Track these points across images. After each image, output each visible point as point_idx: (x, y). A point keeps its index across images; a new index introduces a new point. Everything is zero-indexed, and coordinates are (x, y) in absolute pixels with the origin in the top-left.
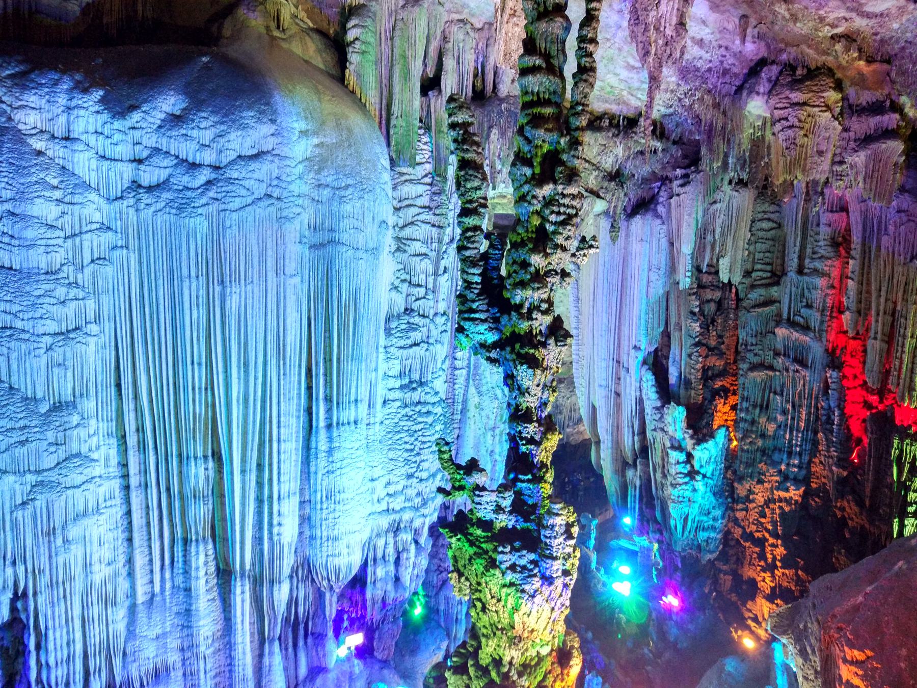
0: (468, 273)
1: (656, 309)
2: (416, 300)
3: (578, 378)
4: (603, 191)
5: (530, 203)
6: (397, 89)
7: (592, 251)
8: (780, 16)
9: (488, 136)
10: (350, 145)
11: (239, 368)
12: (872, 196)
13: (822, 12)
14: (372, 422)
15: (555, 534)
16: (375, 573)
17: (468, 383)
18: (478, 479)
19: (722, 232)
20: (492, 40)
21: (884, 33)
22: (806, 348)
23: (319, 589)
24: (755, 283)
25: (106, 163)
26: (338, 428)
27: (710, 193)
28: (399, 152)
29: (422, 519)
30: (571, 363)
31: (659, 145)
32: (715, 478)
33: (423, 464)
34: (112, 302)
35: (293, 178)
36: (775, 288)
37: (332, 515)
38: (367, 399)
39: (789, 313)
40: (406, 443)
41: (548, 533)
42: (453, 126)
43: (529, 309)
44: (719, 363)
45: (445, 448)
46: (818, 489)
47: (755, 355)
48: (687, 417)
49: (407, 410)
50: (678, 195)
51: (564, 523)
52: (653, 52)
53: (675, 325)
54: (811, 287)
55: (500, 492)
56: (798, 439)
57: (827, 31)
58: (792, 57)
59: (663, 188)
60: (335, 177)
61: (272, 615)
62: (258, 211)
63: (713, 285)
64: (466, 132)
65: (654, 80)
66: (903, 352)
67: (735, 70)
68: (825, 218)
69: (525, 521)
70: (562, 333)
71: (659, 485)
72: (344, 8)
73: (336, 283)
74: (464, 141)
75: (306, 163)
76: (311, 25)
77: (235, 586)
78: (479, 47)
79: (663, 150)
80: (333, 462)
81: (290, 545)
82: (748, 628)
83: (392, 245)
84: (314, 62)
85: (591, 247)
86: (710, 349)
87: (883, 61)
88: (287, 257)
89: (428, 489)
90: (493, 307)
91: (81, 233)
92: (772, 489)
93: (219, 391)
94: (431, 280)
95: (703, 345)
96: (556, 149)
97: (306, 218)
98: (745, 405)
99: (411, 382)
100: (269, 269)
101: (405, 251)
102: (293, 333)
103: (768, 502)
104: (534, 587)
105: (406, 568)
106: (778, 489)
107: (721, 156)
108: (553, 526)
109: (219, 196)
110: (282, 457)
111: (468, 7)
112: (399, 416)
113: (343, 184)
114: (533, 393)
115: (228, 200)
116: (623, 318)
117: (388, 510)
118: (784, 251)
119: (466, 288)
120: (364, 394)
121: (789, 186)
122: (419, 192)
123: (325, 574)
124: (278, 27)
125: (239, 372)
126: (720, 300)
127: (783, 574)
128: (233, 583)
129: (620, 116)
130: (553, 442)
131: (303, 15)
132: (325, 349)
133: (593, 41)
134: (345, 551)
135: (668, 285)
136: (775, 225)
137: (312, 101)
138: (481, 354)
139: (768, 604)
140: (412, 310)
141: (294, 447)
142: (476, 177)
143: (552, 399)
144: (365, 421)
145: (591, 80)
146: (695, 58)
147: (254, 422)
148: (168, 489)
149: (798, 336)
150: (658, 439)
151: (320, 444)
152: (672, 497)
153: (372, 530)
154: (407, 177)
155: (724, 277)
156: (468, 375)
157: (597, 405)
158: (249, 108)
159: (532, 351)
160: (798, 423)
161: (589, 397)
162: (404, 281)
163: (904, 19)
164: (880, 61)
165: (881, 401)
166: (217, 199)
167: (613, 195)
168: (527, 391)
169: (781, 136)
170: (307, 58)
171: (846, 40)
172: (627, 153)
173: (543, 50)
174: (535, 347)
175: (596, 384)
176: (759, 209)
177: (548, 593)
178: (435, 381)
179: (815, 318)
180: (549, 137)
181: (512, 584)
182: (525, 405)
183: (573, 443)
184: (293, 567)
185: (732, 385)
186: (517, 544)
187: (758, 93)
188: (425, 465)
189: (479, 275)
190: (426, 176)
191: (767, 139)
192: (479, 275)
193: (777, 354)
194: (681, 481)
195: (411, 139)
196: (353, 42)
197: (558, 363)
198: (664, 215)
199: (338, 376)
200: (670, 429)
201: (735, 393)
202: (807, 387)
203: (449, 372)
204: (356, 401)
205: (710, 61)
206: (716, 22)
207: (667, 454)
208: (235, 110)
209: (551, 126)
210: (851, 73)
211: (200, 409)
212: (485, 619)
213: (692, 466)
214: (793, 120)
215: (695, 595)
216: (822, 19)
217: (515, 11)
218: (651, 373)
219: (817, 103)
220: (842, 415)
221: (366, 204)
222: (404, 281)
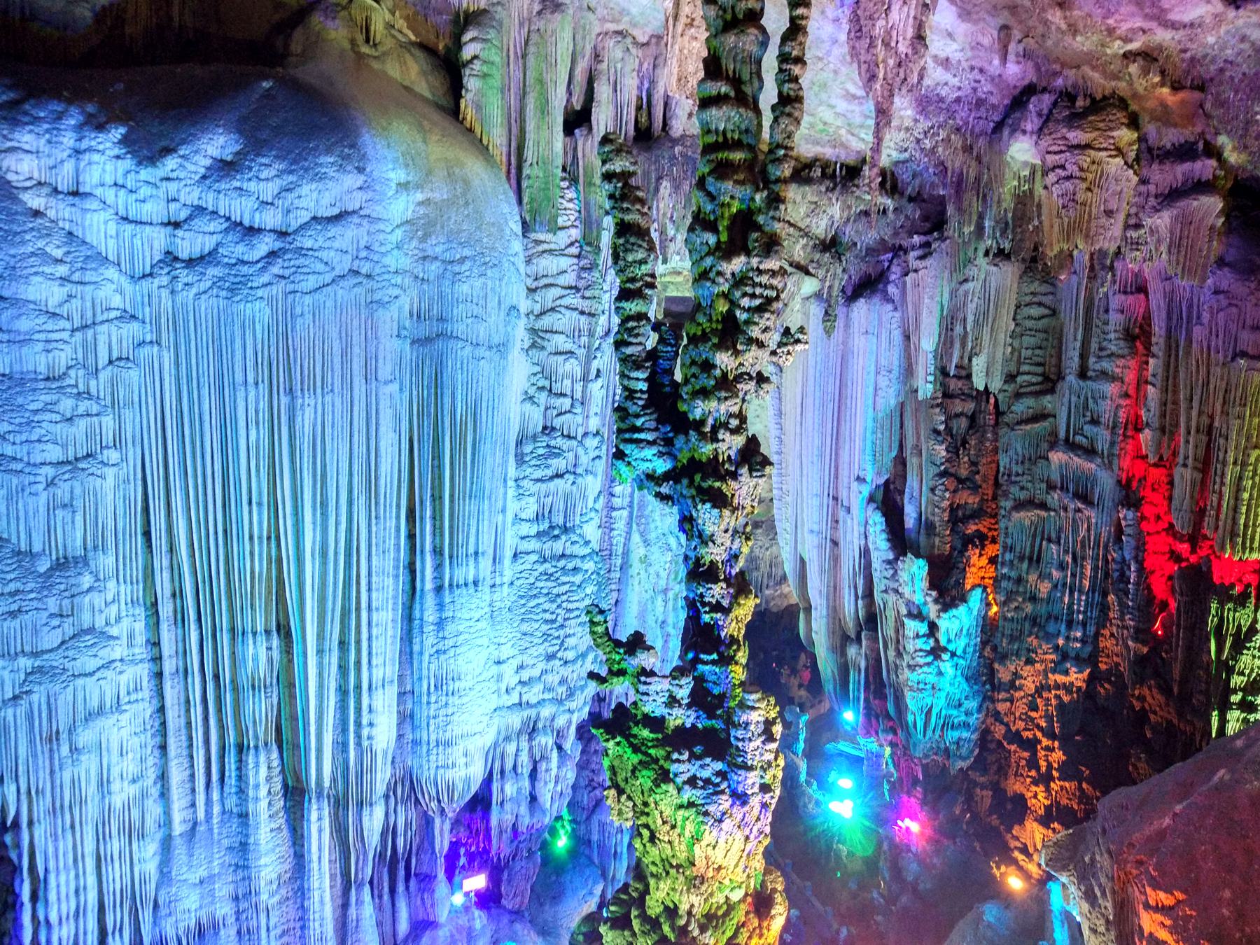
0: (629, 378)
2: (558, 415)
3: (781, 521)
5: (714, 282)
6: (531, 125)
7: (799, 347)
8: (1053, 27)
9: (657, 190)
10: (467, 204)
11: (314, 509)
12: (1179, 271)
13: (1111, 21)
15: (750, 735)
16: (502, 790)
17: (631, 527)
18: (644, 659)
19: (976, 322)
21: (1195, 49)
22: (1093, 480)
24: (1023, 390)
25: (129, 228)
26: (451, 591)
27: (959, 267)
28: (535, 212)
29: (567, 716)
31: (889, 203)
32: (968, 656)
33: (567, 640)
34: (138, 419)
35: (389, 247)
36: (1049, 397)
37: (443, 712)
38: (491, 551)
39: (1068, 431)
40: (545, 611)
42: (608, 177)
43: (713, 427)
44: (972, 500)
45: (599, 618)
46: (1109, 671)
48: (929, 573)
49: (547, 565)
50: (916, 271)
51: (762, 719)
52: (881, 76)
55: (674, 678)
56: (1081, 602)
57: (1117, 47)
58: (1070, 83)
59: (895, 261)
62: (340, 292)
63: (963, 394)
64: (626, 185)
65: (883, 114)
66: (1223, 484)
67: (994, 100)
68: (1116, 301)
70: (759, 459)
71: (892, 666)
72: (458, 14)
73: (447, 393)
74: (624, 197)
75: (407, 227)
76: (413, 38)
79: (895, 209)
80: (444, 638)
81: (385, 753)
83: (526, 339)
84: (417, 89)
85: (798, 341)
86: (960, 481)
87: (1193, 88)
88: (381, 357)
89: (575, 675)
90: (663, 424)
91: (94, 323)
92: (1045, 672)
93: (288, 542)
94: (579, 387)
95: (951, 475)
96: (749, 208)
97: (405, 302)
98: (1008, 556)
99: (552, 528)
100: (356, 372)
101: (543, 348)
103: (1039, 691)
104: (721, 808)
105: (546, 783)
106: (1054, 671)
107: (975, 218)
108: (747, 724)
109: (287, 273)
112: (536, 574)
113: (458, 256)
114: (719, 541)
115: (298, 278)
117: (520, 704)
119: (627, 398)
120: (487, 544)
121: (1067, 258)
122: (562, 266)
123: (434, 793)
124: (367, 41)
125: (314, 515)
127: (1062, 787)
128: (306, 805)
130: (746, 609)
131: (401, 24)
132: (432, 483)
133: (800, 60)
135: (903, 393)
136: (1047, 312)
137: (413, 142)
140: (553, 429)
142: (640, 246)
143: (745, 550)
144: (489, 582)
145: (796, 114)
146: (938, 84)
147: (335, 584)
148: (216, 677)
149: (1079, 462)
151: (426, 614)
153: (499, 732)
154: (545, 246)
155: (979, 382)
157: (807, 560)
158: (328, 151)
159: (717, 484)
160: (1081, 582)
161: (796, 548)
162: (542, 389)
163: (1223, 30)
165: (1193, 551)
166: (283, 277)
167: (827, 271)
169: (1056, 190)
170: (406, 83)
171: (1144, 59)
173: (731, 73)
174: (722, 479)
176: (1027, 290)
177: (740, 816)
178: (585, 526)
179: (1102, 437)
180: (742, 192)
181: (691, 805)
182: (708, 559)
183: (775, 610)
184: (389, 783)
185: (990, 529)
186: (698, 749)
187: (1024, 132)
188: (571, 642)
189: (645, 380)
190: (572, 244)
191: (1036, 194)
192: (645, 380)
193: (1051, 487)
194: (921, 661)
196: (471, 61)
198: (897, 299)
200: (906, 590)
201: (994, 541)
202: (1092, 533)
203: (605, 513)
204: (476, 553)
205: (959, 88)
206: (966, 36)
207: (903, 625)
208: (309, 154)
209: (741, 177)
210: (1150, 104)
211: (260, 566)
213: (937, 641)
214: (1072, 169)
216: (1111, 31)
217: (693, 20)
218: (880, 514)
219: (1104, 145)
220: (1141, 570)
221: (489, 283)
222: (542, 389)
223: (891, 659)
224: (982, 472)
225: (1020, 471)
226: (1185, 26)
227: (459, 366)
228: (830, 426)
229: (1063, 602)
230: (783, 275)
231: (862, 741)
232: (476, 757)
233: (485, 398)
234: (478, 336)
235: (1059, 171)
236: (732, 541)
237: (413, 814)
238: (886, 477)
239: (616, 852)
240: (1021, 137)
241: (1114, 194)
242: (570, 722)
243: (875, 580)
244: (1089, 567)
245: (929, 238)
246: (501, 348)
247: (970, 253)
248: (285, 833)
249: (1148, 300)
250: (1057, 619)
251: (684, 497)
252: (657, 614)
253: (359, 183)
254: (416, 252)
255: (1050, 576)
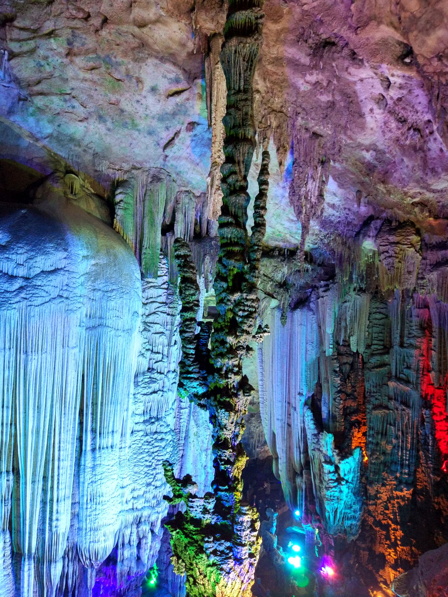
0: (186, 348)
1: (312, 369)
2: (155, 363)
3: (263, 414)
4: (276, 294)
5: (226, 304)
6: (146, 231)
7: (266, 334)
8: (380, 192)
9: (204, 260)
10: (115, 265)
11: (34, 410)
12: (443, 299)
13: (405, 189)
14: (123, 446)
15: (243, 528)
16: (123, 554)
17: (190, 418)
18: (192, 489)
19: (351, 320)
20: (206, 203)
22: (408, 395)
23: (83, 566)
26: (99, 451)
28: (147, 269)
29: (156, 515)
30: (259, 403)
32: (354, 482)
33: (157, 476)
35: (77, 285)
36: (387, 356)
37: (94, 513)
38: (120, 431)
39: (396, 372)
40: (146, 461)
41: (238, 527)
42: (178, 257)
43: (226, 371)
45: (169, 468)
46: (422, 490)
47: (376, 399)
48: (334, 441)
49: (148, 437)
50: (322, 297)
51: (249, 520)
52: (304, 212)
53: (324, 379)
54: (409, 355)
55: (206, 499)
56: (406, 456)
57: (409, 200)
58: (389, 215)
60: (104, 285)
61: (49, 587)
62: (53, 306)
63: (347, 354)
64: (186, 260)
65: (305, 228)
67: (355, 222)
68: (415, 312)
69: (224, 519)
71: (318, 487)
72: (114, 182)
73: (102, 352)
74: (184, 266)
75: (86, 276)
76: (93, 191)
77: (24, 565)
78: (198, 207)
79: (312, 270)
80: (96, 475)
81: (64, 534)
82: (380, 589)
83: (141, 327)
84: (94, 214)
85: (265, 331)
86: (348, 395)
88: (71, 336)
89: (161, 493)
90: (202, 370)
94: (166, 349)
95: (343, 392)
96: (242, 272)
97: (84, 310)
98: (371, 432)
99: (151, 418)
100: (58, 343)
101: (149, 331)
102: (72, 386)
103: (390, 499)
104: (229, 566)
105: (145, 550)
106: (396, 490)
107: (348, 274)
108: (242, 522)
109: (28, 296)
110: (61, 471)
111: (191, 183)
112: (142, 442)
113: (110, 289)
114: (229, 428)
115: (33, 299)
116: (291, 374)
117: (133, 509)
118: (391, 332)
119: (185, 357)
120: (118, 427)
123: (88, 556)
124: (72, 193)
125: (34, 413)
126: (352, 363)
127: (402, 549)
128: (22, 562)
129: (285, 249)
130: (243, 462)
131: (88, 185)
132: (93, 396)
133: (264, 208)
134: (102, 538)
135: (319, 353)
136: (384, 316)
137: (91, 238)
138: (195, 401)
139: (393, 572)
140: (153, 369)
141: (69, 465)
142: (192, 288)
143: (242, 432)
144: (119, 446)
145: (262, 231)
146: (330, 215)
147: (42, 447)
149: (402, 387)
150: (316, 457)
151: (87, 462)
152: (327, 497)
153: (122, 524)
154: (152, 284)
155: (354, 348)
156: (190, 412)
157: (276, 433)
158: (50, 242)
160: (406, 445)
161: (271, 428)
164: (443, 218)
166: (26, 299)
168: (225, 427)
169: (385, 262)
171: (421, 206)
172: (290, 271)
173: (233, 213)
174: (230, 397)
175: (275, 418)
177: (239, 570)
178: (167, 417)
179: (412, 375)
180: (237, 264)
181: (214, 565)
182: (223, 437)
183: (261, 459)
184: (65, 550)
185: (363, 419)
186: (218, 536)
187: (369, 236)
189: (194, 349)
190: (164, 283)
191: (376, 264)
192: (194, 349)
193: (390, 399)
194: (332, 485)
195: (155, 261)
196: (119, 202)
197: (245, 407)
198: (314, 309)
199: (101, 415)
200: (324, 449)
201: (365, 425)
202: (410, 421)
203: (177, 410)
204: (113, 432)
205: (340, 217)
206: (342, 195)
207: (323, 466)
208: (41, 242)
209: (238, 258)
212: (195, 589)
213: (339, 475)
215: (344, 565)
216: (406, 193)
218: (310, 411)
219: (406, 243)
220: (434, 439)
221: (125, 301)
223: (317, 484)
224: (358, 391)
225: (375, 391)
226: (439, 192)
227: (108, 339)
228: (285, 368)
229: (398, 454)
230: (257, 302)
231: (304, 526)
232: (110, 537)
233: (120, 355)
234: (118, 325)
235: (386, 254)
236: (235, 428)
237: (77, 568)
238: (313, 393)
239: (180, 586)
240: (368, 239)
241: (411, 264)
242: (158, 518)
243: (309, 444)
244: (410, 438)
245: (328, 283)
246: (129, 331)
247: (347, 290)
248: (11, 577)
249: (429, 312)
250: (396, 463)
251: (212, 406)
252: (202, 462)
253: (65, 256)
254: (90, 287)
255: (391, 442)
